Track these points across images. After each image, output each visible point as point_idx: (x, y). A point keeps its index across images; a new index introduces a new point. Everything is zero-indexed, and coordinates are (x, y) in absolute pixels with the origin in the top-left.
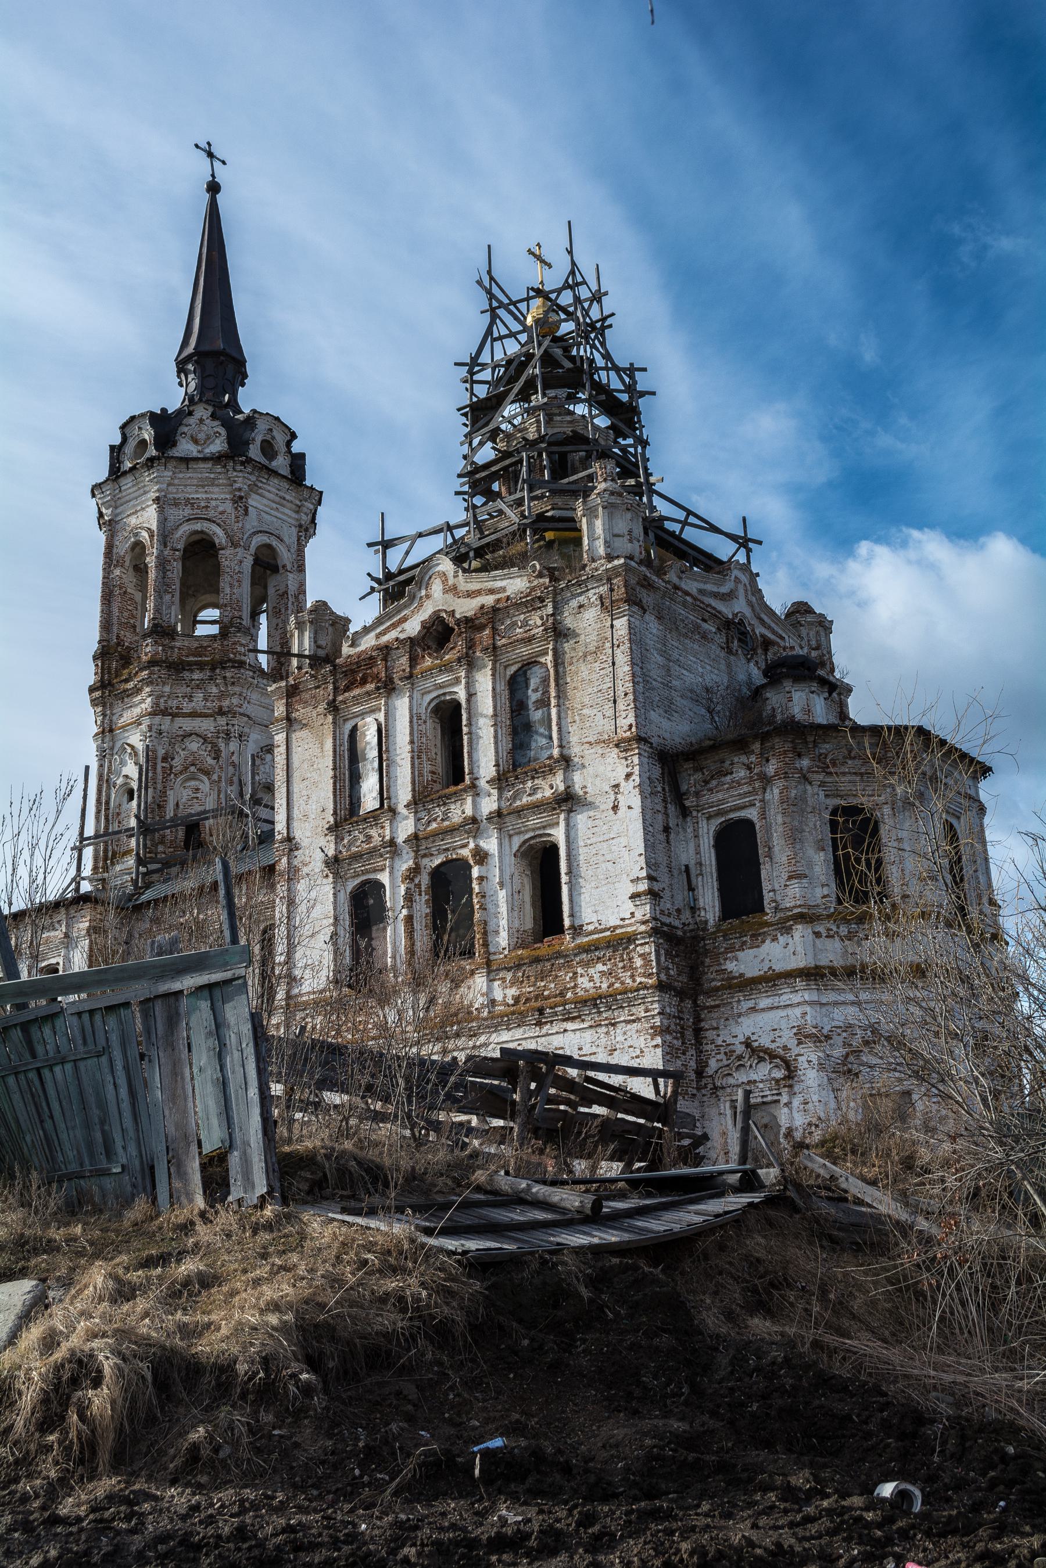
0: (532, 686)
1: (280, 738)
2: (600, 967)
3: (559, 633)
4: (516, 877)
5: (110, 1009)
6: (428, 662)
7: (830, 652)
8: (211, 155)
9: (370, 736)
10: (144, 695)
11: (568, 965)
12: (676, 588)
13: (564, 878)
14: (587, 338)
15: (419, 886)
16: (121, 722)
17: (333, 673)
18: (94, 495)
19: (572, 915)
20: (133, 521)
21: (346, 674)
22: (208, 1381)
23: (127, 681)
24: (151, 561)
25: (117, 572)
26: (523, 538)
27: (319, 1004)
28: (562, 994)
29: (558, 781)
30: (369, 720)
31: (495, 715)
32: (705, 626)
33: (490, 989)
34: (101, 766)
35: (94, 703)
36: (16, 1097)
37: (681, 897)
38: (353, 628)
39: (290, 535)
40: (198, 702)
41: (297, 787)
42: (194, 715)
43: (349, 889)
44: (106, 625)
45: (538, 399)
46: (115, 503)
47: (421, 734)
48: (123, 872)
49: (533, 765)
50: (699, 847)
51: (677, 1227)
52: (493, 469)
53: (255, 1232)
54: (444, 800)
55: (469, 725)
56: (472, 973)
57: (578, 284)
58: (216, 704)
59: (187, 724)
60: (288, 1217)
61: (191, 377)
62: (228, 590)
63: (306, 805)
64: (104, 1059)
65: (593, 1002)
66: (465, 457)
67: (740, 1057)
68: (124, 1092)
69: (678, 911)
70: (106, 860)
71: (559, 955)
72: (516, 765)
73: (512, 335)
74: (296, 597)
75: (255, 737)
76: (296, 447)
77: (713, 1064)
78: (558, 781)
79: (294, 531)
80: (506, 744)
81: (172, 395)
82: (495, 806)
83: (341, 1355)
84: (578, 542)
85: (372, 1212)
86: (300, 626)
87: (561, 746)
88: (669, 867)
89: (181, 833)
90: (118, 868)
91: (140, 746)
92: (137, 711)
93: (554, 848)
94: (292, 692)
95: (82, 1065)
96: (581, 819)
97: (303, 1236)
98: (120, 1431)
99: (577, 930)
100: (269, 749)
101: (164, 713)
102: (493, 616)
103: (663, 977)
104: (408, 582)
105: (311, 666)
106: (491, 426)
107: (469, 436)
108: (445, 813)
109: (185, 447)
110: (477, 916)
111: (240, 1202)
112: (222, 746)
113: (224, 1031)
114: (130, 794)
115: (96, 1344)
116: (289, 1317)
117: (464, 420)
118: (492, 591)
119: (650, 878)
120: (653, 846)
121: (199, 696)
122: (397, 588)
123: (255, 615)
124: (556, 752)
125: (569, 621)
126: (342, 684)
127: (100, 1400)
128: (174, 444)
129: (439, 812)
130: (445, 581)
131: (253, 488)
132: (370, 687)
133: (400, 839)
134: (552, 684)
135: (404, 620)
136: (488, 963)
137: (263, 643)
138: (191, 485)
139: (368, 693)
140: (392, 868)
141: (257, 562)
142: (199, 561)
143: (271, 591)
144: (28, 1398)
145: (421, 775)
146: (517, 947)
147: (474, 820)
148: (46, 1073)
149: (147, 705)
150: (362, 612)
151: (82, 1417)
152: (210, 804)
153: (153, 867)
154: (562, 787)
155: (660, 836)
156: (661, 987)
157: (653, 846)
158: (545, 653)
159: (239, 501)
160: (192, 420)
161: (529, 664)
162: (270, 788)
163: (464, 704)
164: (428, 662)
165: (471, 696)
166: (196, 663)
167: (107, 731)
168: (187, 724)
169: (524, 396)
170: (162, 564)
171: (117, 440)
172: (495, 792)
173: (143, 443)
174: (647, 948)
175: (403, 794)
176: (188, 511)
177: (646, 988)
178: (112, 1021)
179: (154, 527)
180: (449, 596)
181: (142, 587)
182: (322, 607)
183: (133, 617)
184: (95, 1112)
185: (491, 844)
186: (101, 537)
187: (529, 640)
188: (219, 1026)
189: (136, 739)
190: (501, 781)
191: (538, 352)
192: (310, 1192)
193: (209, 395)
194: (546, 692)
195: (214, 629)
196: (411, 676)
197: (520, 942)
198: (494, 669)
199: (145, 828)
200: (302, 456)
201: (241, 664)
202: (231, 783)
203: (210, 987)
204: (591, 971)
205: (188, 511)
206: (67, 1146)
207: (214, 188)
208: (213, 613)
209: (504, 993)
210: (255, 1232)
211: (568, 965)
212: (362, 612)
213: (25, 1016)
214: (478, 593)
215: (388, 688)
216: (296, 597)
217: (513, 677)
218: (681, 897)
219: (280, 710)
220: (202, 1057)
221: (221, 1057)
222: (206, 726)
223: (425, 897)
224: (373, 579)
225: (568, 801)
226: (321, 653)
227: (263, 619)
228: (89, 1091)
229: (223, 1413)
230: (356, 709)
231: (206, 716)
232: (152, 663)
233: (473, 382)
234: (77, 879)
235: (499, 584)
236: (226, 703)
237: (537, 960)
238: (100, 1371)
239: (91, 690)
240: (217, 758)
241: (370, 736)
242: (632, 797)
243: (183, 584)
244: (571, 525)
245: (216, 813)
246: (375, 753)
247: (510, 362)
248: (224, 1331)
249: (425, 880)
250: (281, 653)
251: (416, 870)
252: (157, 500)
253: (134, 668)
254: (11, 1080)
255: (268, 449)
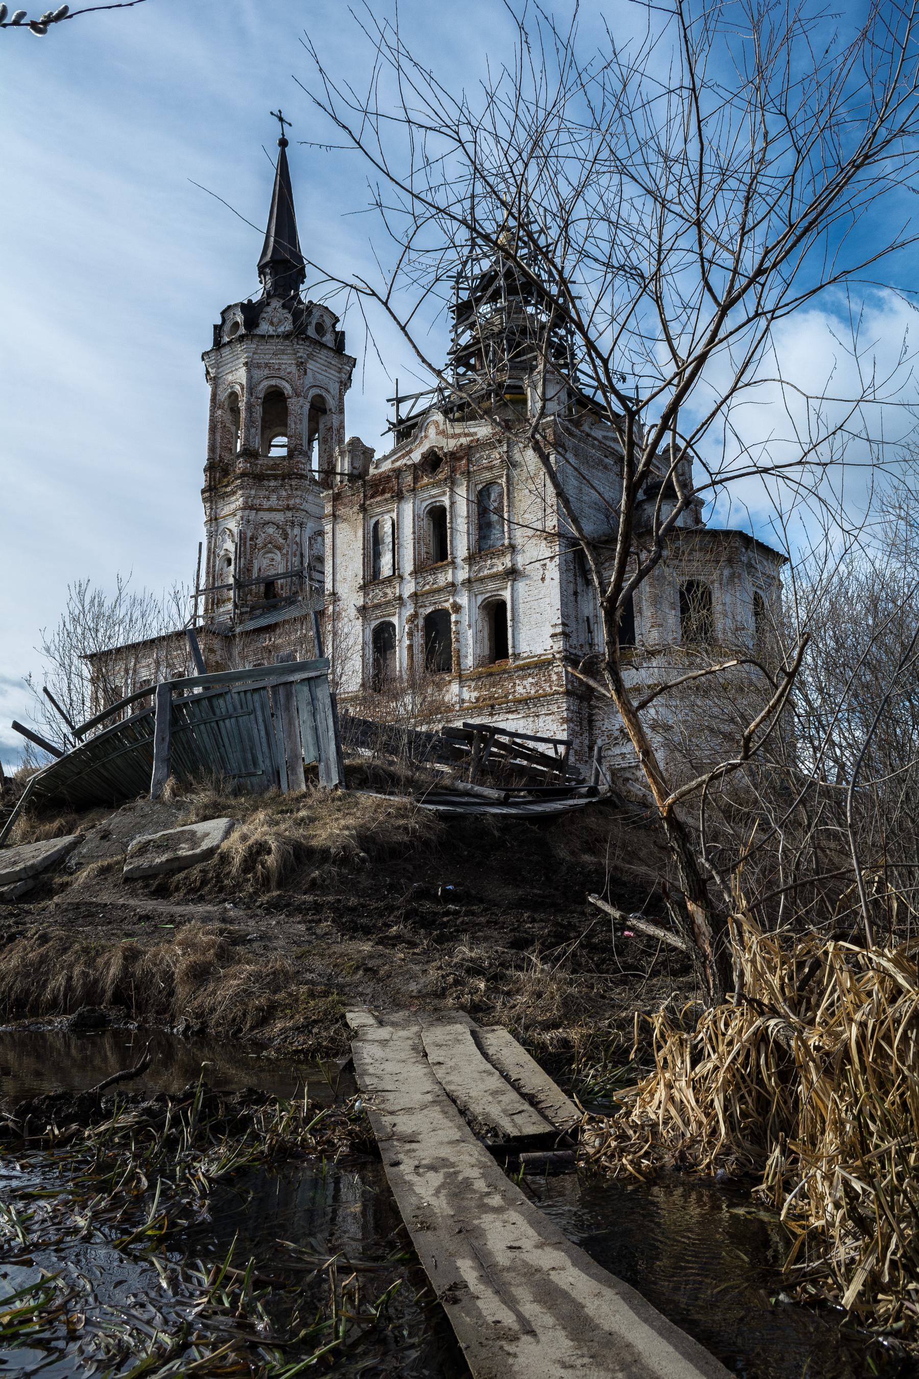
0: (492, 498)
1: (328, 528)
2: (530, 680)
3: (510, 463)
4: (479, 622)
5: (255, 690)
6: (426, 480)
7: (691, 478)
8: (281, 119)
9: (387, 528)
10: (238, 496)
11: (510, 678)
12: (588, 435)
13: (509, 623)
14: (536, 259)
15: (417, 626)
16: (223, 513)
17: (364, 486)
18: (203, 359)
19: (513, 647)
20: (230, 378)
21: (371, 486)
22: (317, 856)
23: (226, 486)
24: (242, 405)
25: (219, 412)
26: (489, 398)
27: (353, 699)
28: (506, 696)
29: (507, 561)
30: (387, 517)
31: (468, 517)
32: (606, 460)
33: (461, 692)
34: (210, 542)
35: (205, 500)
36: (205, 736)
37: (583, 637)
38: (377, 456)
39: (334, 388)
40: (273, 501)
41: (338, 560)
42: (271, 510)
43: (372, 627)
44: (212, 449)
45: (502, 303)
46: (217, 365)
47: (420, 528)
48: (225, 613)
49: (492, 550)
50: (593, 606)
51: (548, 810)
52: (471, 350)
53: (333, 801)
54: (434, 571)
55: (451, 522)
56: (450, 682)
57: (531, 223)
58: (285, 503)
59: (267, 516)
60: (349, 795)
61: (268, 277)
62: (293, 426)
63: (345, 570)
64: (252, 716)
65: (525, 701)
66: (452, 340)
67: (616, 738)
68: (263, 733)
69: (581, 645)
70: (214, 603)
71: (505, 671)
72: (482, 549)
73: (486, 256)
74: (338, 431)
75: (311, 526)
76: (338, 328)
77: (599, 742)
78: (507, 561)
79: (337, 385)
80: (474, 538)
81: (253, 289)
82: (467, 576)
83: (378, 852)
84: (525, 402)
85: (391, 794)
86: (342, 453)
87: (510, 538)
88: (576, 617)
89: (262, 588)
90: (221, 610)
91: (235, 530)
92: (233, 506)
93: (504, 603)
94: (337, 498)
95: (240, 719)
96: (521, 585)
97: (357, 804)
98: (280, 873)
99: (516, 656)
100: (321, 533)
101: (251, 508)
102: (467, 452)
103: (570, 687)
104: (414, 426)
105: (349, 481)
106: (470, 320)
107: (455, 327)
108: (434, 580)
109: (264, 328)
110: (454, 646)
111: (325, 788)
112: (289, 531)
113: (316, 702)
114: (229, 561)
115: (267, 837)
116: (354, 832)
117: (452, 315)
118: (466, 435)
119: (563, 624)
120: (566, 604)
121: (274, 497)
122: (405, 430)
123: (310, 441)
124: (506, 542)
125: (517, 457)
126: (369, 493)
127: (271, 860)
128: (257, 326)
129: (430, 579)
130: (437, 427)
131: (310, 356)
132: (388, 495)
133: (406, 595)
134: (505, 497)
135: (411, 451)
136: (460, 676)
137: (315, 466)
138: (266, 353)
139: (386, 500)
140: (400, 614)
141: (313, 406)
142: (273, 408)
143: (321, 426)
144: (237, 860)
145: (419, 554)
146: (478, 666)
147: (453, 584)
148: (221, 723)
149: (240, 502)
150: (383, 445)
151: (263, 867)
152: (281, 569)
153: (244, 610)
154: (509, 565)
155: (571, 597)
156: (568, 693)
157: (566, 604)
158: (501, 477)
159: (301, 365)
160: (269, 309)
161: (490, 484)
162: (320, 559)
163: (448, 507)
164: (426, 480)
165: (453, 503)
166: (272, 475)
167: (213, 520)
168: (267, 516)
169: (494, 298)
170: (250, 407)
171: (219, 322)
172: (467, 567)
173: (236, 324)
174: (560, 669)
175: (408, 566)
176: (266, 372)
177: (558, 693)
178: (256, 697)
179: (244, 382)
180: (440, 437)
181: (236, 423)
182: (356, 441)
183: (230, 443)
184: (247, 744)
185: (463, 600)
186: (208, 389)
187: (491, 468)
188: (313, 700)
189: (233, 525)
190: (471, 559)
191: (502, 270)
192: (360, 784)
193: (280, 290)
194: (501, 502)
195: (283, 452)
196: (414, 490)
197: (481, 662)
198: (468, 486)
199: (239, 585)
200: (343, 333)
201: (302, 477)
202: (295, 556)
203: (309, 679)
204: (525, 682)
205: (266, 372)
206: (232, 761)
207: (283, 143)
208: (283, 440)
209: (469, 695)
210: (333, 801)
211: (510, 678)
212: (383, 445)
213: (212, 693)
214: (459, 436)
215: (399, 496)
216: (338, 431)
217: (480, 492)
218: (583, 637)
219: (328, 509)
220: (305, 715)
221: (314, 715)
222: (279, 517)
223: (421, 633)
224: (390, 423)
225: (513, 573)
226: (356, 472)
227: (316, 444)
228: (244, 732)
229: (326, 866)
230: (378, 510)
231: (278, 510)
232: (243, 475)
233: (459, 289)
234: (195, 617)
235: (472, 430)
236: (292, 502)
237: (491, 675)
238: (270, 848)
239: (203, 492)
240: (285, 539)
241: (387, 528)
242: (553, 572)
243: (263, 419)
244: (518, 390)
245: (285, 575)
246: (390, 539)
247: (484, 276)
248: (324, 836)
249: (421, 622)
250: (329, 471)
251: (415, 616)
252: (246, 364)
253: (231, 477)
254: (202, 727)
255: (320, 328)
